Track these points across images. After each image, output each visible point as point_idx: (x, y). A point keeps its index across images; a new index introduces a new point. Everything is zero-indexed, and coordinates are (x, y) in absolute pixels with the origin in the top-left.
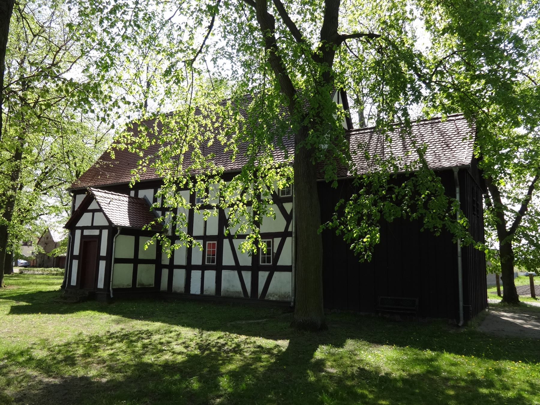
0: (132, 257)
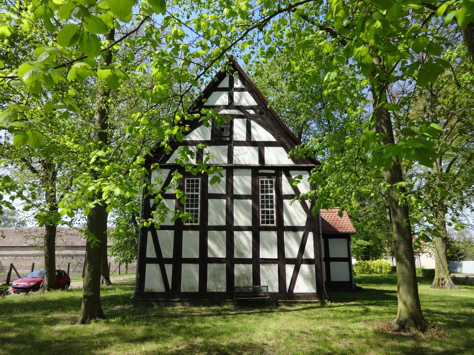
0: (184, 256)
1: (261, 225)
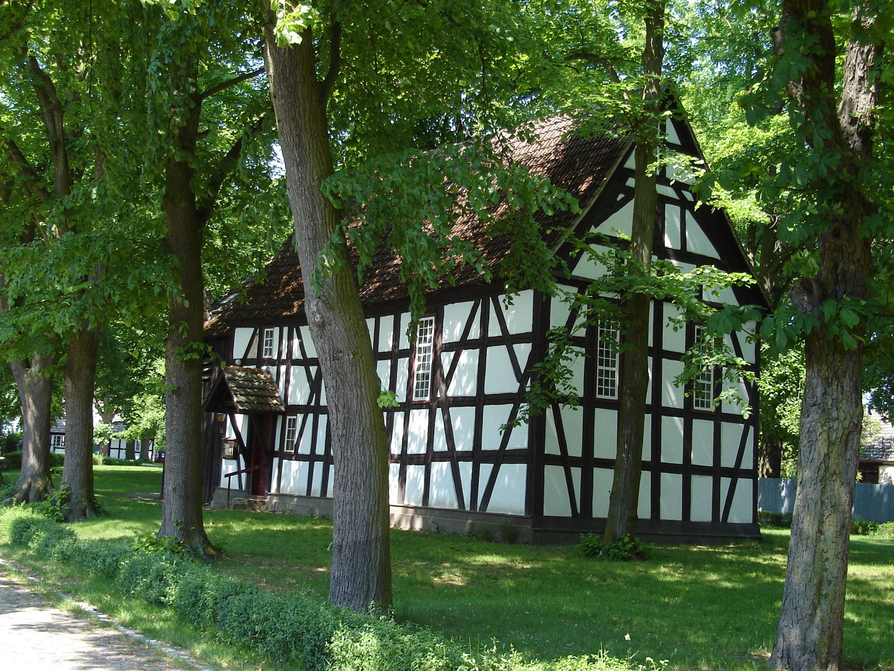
1: (598, 396)
